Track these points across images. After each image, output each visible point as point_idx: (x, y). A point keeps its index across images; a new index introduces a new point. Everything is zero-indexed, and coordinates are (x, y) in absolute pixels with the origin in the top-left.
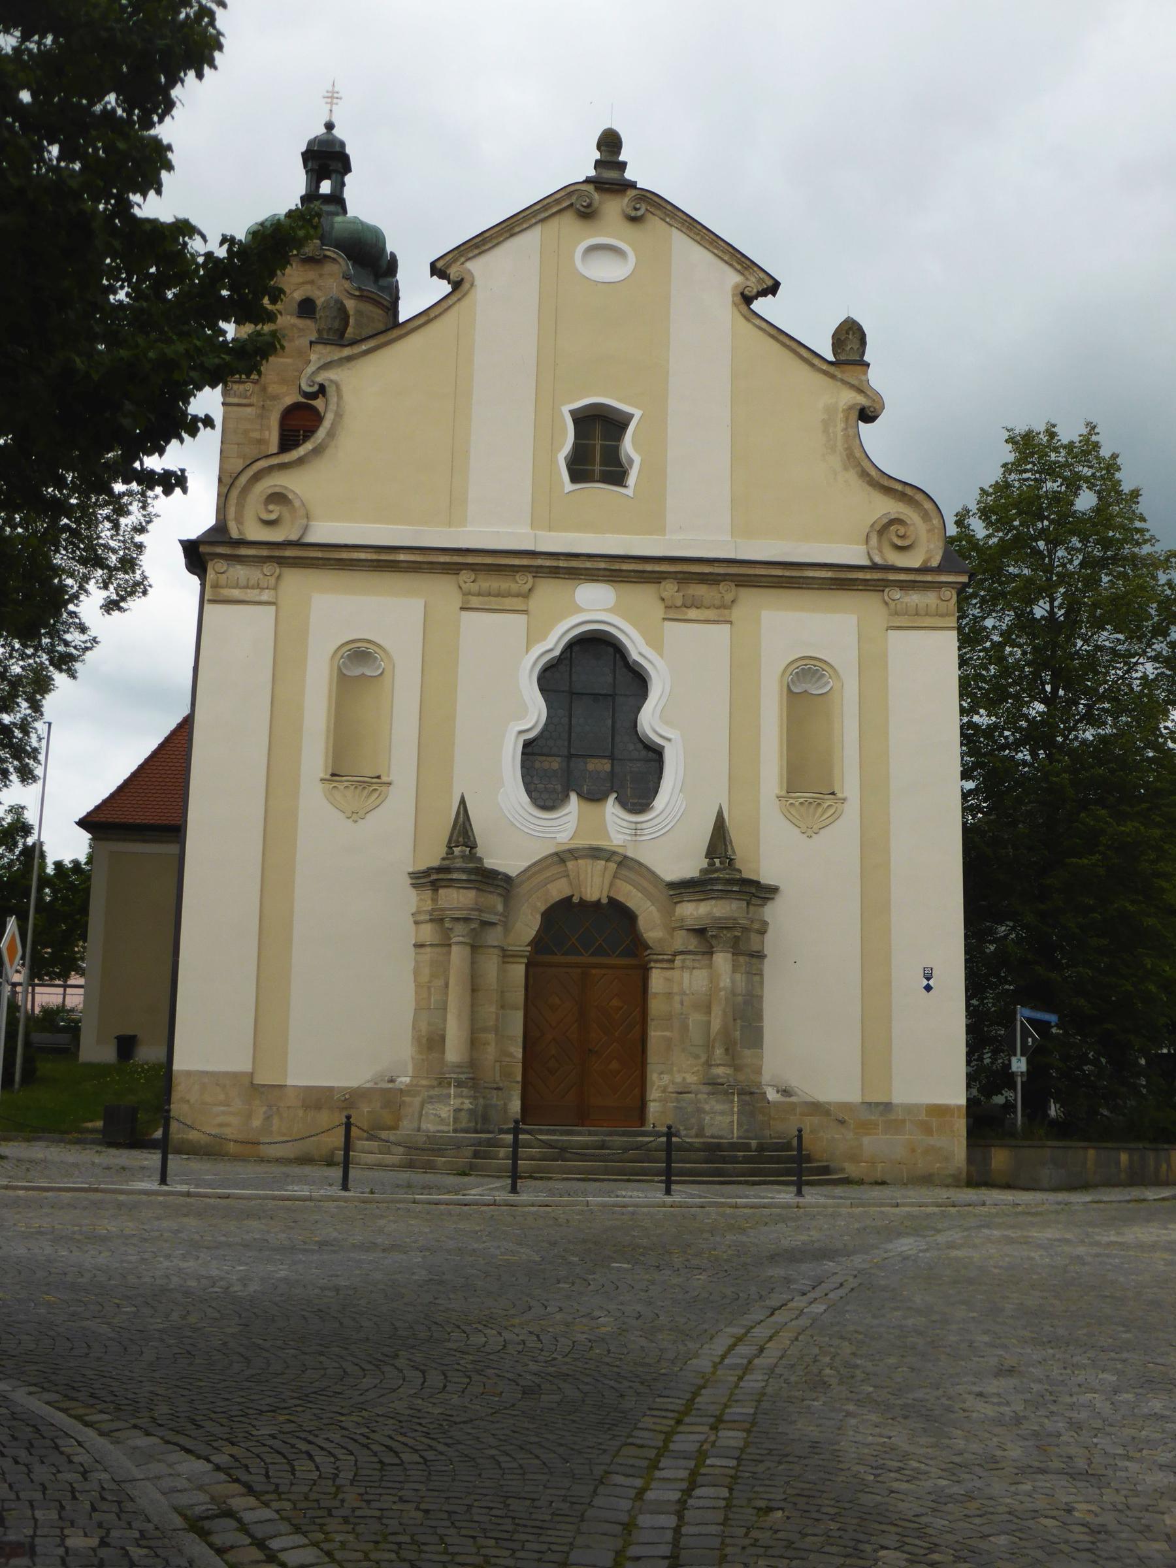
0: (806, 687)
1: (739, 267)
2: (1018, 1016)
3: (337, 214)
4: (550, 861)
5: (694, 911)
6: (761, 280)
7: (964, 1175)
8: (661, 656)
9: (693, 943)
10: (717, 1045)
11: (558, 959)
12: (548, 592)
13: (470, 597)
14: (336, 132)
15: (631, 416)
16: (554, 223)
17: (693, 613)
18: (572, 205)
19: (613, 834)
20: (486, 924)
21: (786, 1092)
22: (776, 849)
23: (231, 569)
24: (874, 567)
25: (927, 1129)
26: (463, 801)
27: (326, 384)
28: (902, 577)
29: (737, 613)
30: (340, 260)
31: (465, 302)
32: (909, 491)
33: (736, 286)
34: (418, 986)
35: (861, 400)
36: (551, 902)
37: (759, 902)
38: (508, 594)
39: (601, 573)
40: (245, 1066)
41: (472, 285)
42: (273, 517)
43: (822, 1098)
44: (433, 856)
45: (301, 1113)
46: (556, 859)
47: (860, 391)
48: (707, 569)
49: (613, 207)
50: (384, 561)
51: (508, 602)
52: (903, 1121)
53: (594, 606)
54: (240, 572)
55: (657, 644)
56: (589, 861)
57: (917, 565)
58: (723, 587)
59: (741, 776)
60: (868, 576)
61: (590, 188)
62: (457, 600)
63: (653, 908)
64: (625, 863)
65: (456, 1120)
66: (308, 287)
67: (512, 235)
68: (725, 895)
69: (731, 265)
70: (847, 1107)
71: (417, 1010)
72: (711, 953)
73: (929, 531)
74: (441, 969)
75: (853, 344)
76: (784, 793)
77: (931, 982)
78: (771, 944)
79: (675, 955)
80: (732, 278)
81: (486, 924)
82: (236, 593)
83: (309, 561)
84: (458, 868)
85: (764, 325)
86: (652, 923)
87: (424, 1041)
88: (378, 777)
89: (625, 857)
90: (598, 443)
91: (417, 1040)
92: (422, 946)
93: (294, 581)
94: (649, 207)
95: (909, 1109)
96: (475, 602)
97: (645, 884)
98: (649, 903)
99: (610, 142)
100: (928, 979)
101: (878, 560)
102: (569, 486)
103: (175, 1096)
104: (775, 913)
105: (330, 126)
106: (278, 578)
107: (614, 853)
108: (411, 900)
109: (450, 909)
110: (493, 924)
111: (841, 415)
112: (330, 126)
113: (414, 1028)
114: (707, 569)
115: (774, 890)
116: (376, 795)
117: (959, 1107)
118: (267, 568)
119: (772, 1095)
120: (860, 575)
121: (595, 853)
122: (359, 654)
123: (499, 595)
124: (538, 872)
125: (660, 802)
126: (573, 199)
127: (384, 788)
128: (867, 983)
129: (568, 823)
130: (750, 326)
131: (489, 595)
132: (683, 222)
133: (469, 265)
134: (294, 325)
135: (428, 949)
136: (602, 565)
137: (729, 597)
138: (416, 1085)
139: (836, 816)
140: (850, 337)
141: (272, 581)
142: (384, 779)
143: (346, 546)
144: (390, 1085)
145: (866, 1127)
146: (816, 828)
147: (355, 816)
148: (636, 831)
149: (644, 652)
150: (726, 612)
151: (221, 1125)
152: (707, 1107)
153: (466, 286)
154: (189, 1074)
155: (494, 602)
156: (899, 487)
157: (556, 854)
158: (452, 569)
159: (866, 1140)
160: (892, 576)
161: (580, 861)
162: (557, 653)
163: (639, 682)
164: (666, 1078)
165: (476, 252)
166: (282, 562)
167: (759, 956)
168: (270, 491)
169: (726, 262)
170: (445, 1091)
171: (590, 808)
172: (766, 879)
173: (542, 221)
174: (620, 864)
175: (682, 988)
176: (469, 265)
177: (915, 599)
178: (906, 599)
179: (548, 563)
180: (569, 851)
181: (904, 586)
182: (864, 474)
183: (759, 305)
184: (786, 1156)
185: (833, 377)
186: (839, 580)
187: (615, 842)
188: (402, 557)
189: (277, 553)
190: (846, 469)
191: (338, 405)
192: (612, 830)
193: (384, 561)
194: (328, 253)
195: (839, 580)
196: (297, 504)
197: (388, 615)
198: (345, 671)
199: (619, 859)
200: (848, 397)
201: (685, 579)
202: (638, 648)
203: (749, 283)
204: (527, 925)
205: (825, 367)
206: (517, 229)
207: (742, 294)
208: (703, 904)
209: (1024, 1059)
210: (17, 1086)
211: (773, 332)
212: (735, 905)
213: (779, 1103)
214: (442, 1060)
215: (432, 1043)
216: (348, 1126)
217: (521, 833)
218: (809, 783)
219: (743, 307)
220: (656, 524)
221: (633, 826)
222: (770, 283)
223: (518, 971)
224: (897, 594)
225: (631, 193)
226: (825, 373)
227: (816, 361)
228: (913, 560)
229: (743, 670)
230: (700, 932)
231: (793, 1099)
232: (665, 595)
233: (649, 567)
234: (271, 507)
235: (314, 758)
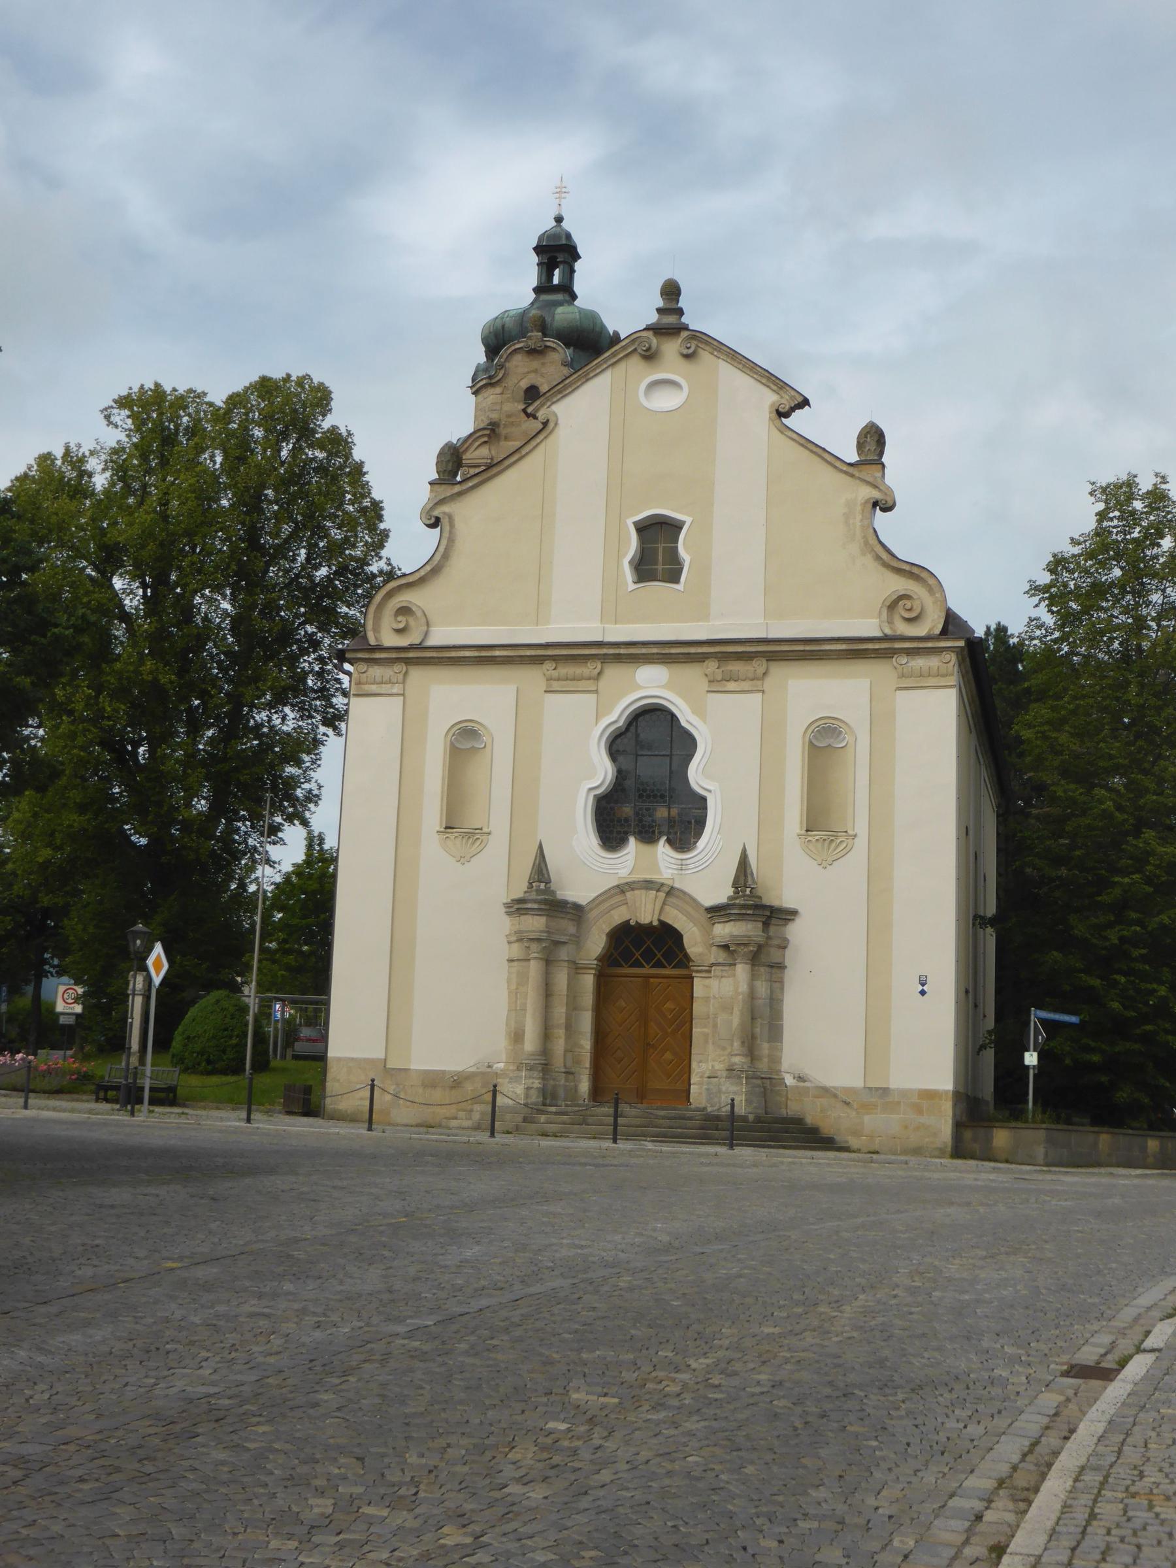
0: (824, 742)
1: (775, 388)
2: (1032, 1017)
3: (561, 304)
5: (724, 930)
6: (792, 398)
7: (949, 1149)
8: (705, 722)
9: (722, 956)
11: (627, 970)
12: (614, 674)
14: (565, 225)
15: (684, 522)
16: (622, 366)
17: (732, 686)
18: (635, 350)
19: (663, 870)
20: (557, 943)
21: (800, 1079)
22: (793, 881)
24: (886, 638)
25: (919, 1110)
26: (541, 847)
27: (441, 516)
29: (768, 683)
30: (559, 349)
32: (915, 570)
33: (772, 405)
35: (876, 495)
36: (615, 924)
37: (780, 922)
38: (581, 678)
40: (380, 1055)
41: (556, 424)
42: (401, 626)
43: (830, 1082)
44: (519, 891)
45: (421, 1090)
47: (875, 487)
49: (671, 348)
51: (582, 685)
52: (899, 1103)
53: (652, 683)
54: (376, 671)
55: (700, 711)
56: (643, 892)
58: (756, 663)
59: (768, 819)
60: (877, 646)
61: (650, 334)
62: (543, 685)
63: (695, 929)
65: (527, 1096)
66: (532, 375)
67: (587, 380)
68: (741, 917)
70: (848, 1090)
73: (934, 603)
74: (522, 979)
75: (872, 445)
76: (803, 832)
77: (925, 988)
78: (790, 956)
79: (713, 965)
80: (769, 398)
81: (557, 943)
82: (374, 688)
84: (544, 903)
85: (795, 436)
86: (695, 942)
89: (672, 887)
90: (657, 549)
92: (512, 961)
93: (417, 675)
94: (698, 345)
95: (904, 1093)
96: (556, 685)
97: (690, 909)
98: (691, 925)
99: (671, 291)
100: (923, 985)
101: (888, 631)
102: (632, 587)
103: (330, 1076)
104: (795, 931)
105: (559, 220)
106: (406, 673)
107: (663, 884)
108: (506, 924)
110: (564, 943)
111: (859, 508)
112: (559, 220)
114: (740, 649)
115: (794, 913)
116: (478, 842)
117: (946, 1092)
119: (789, 1081)
120: (870, 646)
121: (648, 885)
124: (604, 901)
125: (701, 844)
127: (484, 837)
128: (878, 989)
130: (783, 437)
131: (567, 679)
132: (728, 354)
133: (555, 408)
136: (655, 650)
137: (761, 670)
140: (873, 440)
141: (401, 677)
142: (485, 830)
145: (867, 1107)
146: (830, 860)
147: (462, 859)
149: (691, 720)
150: (759, 683)
153: (551, 425)
154: (339, 1059)
155: (571, 685)
156: (907, 567)
157: (617, 886)
160: (897, 645)
161: (636, 892)
162: (621, 723)
163: (688, 743)
164: (703, 1065)
166: (408, 662)
167: (780, 967)
168: (398, 606)
171: (645, 849)
172: (788, 902)
174: (668, 894)
175: (719, 993)
177: (919, 663)
179: (611, 651)
180: (627, 884)
181: (910, 652)
183: (793, 421)
184: (780, 1126)
185: (852, 476)
186: (854, 650)
187: (665, 876)
188: (497, 653)
189: (403, 655)
190: (863, 554)
191: (450, 532)
194: (548, 344)
195: (854, 650)
197: (486, 699)
198: (458, 745)
199: (667, 889)
200: (867, 493)
201: (724, 658)
202: (687, 717)
203: (783, 401)
204: (596, 944)
205: (845, 468)
207: (777, 411)
209: (1035, 1054)
210: (247, 1072)
211: (802, 441)
212: (750, 926)
213: (797, 1087)
215: (517, 1037)
216: (373, 1086)
217: (590, 870)
218: (821, 821)
219: (777, 422)
222: (800, 399)
223: (588, 981)
224: (903, 659)
225: (684, 334)
226: (846, 473)
227: (838, 464)
228: (920, 630)
229: (771, 730)
230: (726, 947)
231: (807, 1084)
233: (693, 650)
234: (399, 618)
235: (432, 815)
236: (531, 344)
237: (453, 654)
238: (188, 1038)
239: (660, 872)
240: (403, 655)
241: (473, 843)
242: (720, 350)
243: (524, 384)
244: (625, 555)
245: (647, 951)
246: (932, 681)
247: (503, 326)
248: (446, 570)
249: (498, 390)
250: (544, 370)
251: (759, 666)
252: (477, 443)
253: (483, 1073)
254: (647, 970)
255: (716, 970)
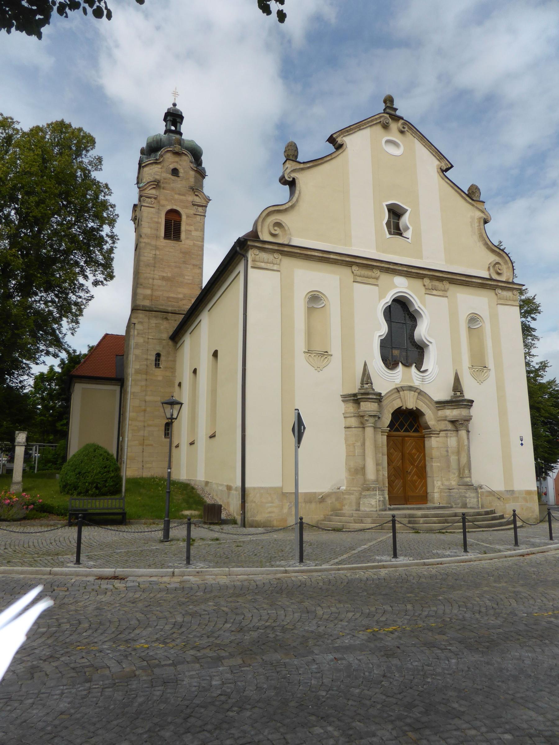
4: (394, 391)
9: (450, 426)
10: (466, 469)
12: (385, 278)
13: (357, 277)
15: (407, 210)
17: (435, 292)
18: (380, 122)
19: (415, 381)
23: (260, 254)
25: (526, 500)
26: (365, 365)
28: (503, 285)
29: (449, 294)
31: (344, 153)
33: (438, 165)
34: (348, 445)
39: (404, 272)
40: (279, 484)
46: (396, 390)
47: (483, 212)
48: (441, 275)
50: (325, 258)
51: (371, 281)
52: (518, 497)
53: (401, 286)
54: (264, 256)
56: (408, 392)
57: (504, 280)
63: (430, 412)
64: (421, 393)
67: (360, 130)
69: (435, 157)
71: (347, 456)
72: (457, 431)
77: (523, 442)
82: (263, 265)
83: (294, 254)
86: (430, 417)
87: (353, 470)
88: (327, 352)
91: (349, 470)
93: (287, 262)
95: (520, 492)
96: (359, 279)
97: (427, 402)
100: (522, 441)
105: (175, 105)
108: (341, 407)
109: (369, 411)
112: (175, 105)
113: (346, 464)
114: (441, 275)
116: (326, 360)
117: (535, 491)
118: (276, 255)
121: (411, 388)
122: (315, 298)
123: (367, 277)
124: (389, 396)
126: (382, 120)
129: (400, 375)
131: (364, 277)
134: (170, 178)
135: (354, 429)
136: (405, 269)
138: (350, 490)
139: (488, 377)
141: (278, 261)
143: (310, 249)
144: (338, 491)
146: (482, 380)
147: (319, 369)
148: (423, 380)
151: (270, 513)
152: (467, 495)
154: (254, 488)
155: (365, 280)
157: (397, 388)
158: (349, 264)
159: (507, 505)
165: (347, 134)
166: (282, 253)
168: (276, 221)
169: (434, 155)
170: (374, 492)
171: (406, 369)
173: (370, 126)
176: (344, 138)
178: (503, 293)
180: (401, 387)
181: (503, 288)
182: (486, 244)
185: (473, 205)
187: (416, 384)
189: (281, 249)
192: (414, 378)
193: (325, 258)
196: (286, 228)
199: (418, 391)
206: (362, 128)
208: (455, 410)
214: (365, 480)
219: (441, 174)
220: (420, 256)
221: (422, 378)
224: (500, 291)
230: (453, 422)
232: (425, 284)
234: (276, 228)
235: (300, 344)
236: (177, 150)
237: (309, 253)
238: (79, 473)
239: (414, 383)
240: (281, 249)
241: (324, 360)
242: (416, 134)
243: (172, 167)
244: (384, 220)
245: (407, 423)
246: (510, 303)
247: (161, 139)
248: (297, 208)
249: (159, 166)
250: (181, 163)
251: (446, 284)
252: (151, 187)
253: (335, 493)
254: (402, 433)
255: (442, 434)
